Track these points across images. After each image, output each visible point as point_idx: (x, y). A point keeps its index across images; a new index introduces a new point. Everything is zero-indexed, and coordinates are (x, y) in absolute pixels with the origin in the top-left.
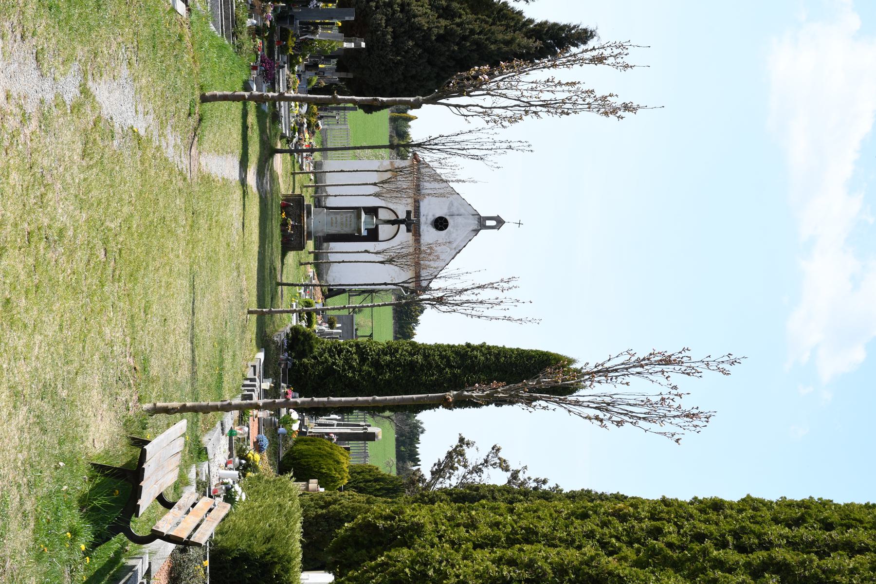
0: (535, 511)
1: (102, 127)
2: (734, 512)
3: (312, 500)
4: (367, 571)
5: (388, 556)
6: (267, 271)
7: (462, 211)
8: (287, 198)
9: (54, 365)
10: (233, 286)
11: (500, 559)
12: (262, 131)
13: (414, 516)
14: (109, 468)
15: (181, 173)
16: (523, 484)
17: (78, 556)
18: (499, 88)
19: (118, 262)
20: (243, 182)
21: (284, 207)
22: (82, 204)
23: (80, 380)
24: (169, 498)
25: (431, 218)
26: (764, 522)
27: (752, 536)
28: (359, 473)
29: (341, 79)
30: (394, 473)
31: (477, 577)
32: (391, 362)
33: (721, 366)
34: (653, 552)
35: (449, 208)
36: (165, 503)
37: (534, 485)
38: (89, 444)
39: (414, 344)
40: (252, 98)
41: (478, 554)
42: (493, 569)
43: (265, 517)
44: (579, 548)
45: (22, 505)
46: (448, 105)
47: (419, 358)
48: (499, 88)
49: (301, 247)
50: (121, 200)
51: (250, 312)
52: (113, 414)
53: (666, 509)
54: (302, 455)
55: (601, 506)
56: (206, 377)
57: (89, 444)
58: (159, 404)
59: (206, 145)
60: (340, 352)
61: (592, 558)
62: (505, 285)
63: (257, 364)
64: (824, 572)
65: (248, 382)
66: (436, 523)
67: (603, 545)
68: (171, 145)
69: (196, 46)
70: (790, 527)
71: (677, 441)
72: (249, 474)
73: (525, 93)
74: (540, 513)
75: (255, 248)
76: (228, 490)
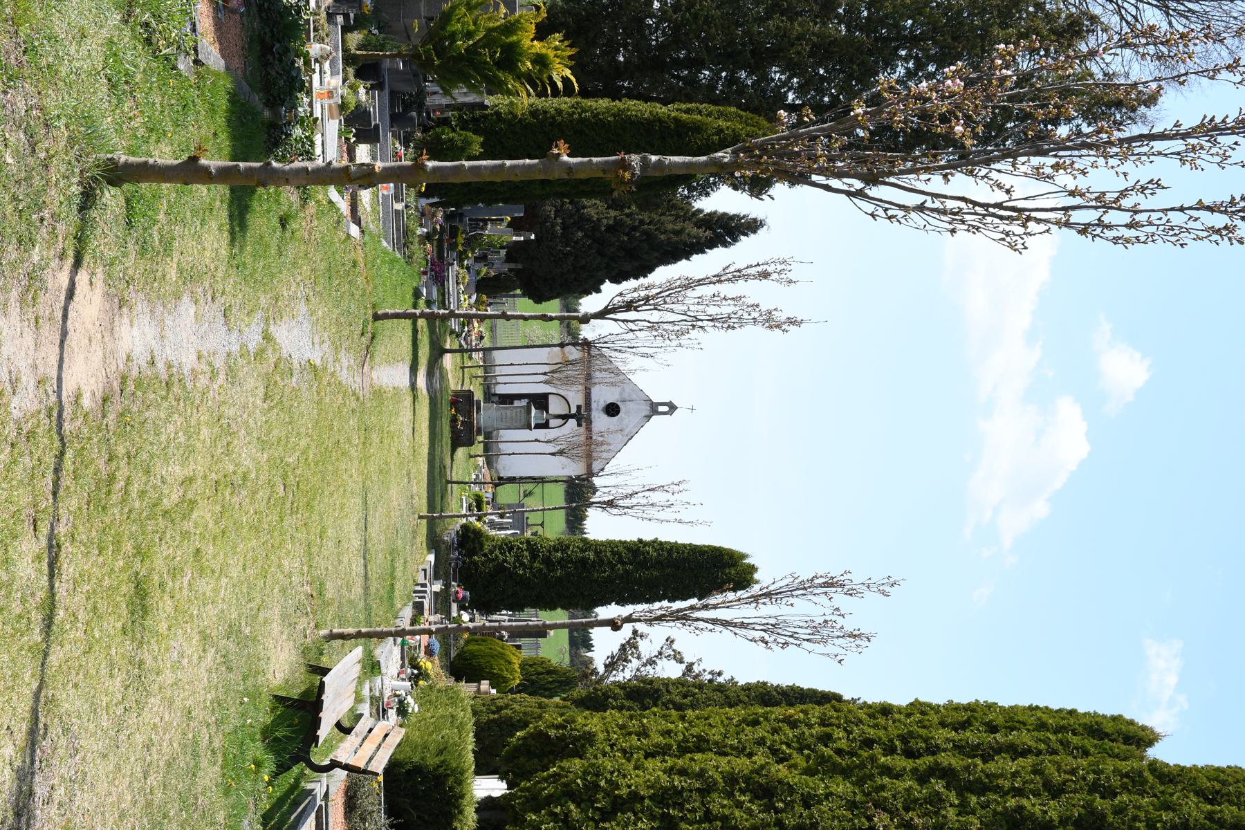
0: (706, 719)
1: (283, 367)
2: (902, 717)
3: (484, 705)
4: (539, 782)
5: (560, 767)
6: (437, 471)
7: (634, 397)
8: (457, 394)
9: (239, 604)
10: (405, 492)
11: (672, 768)
12: (432, 332)
13: (586, 725)
14: (290, 699)
15: (354, 394)
16: (697, 676)
17: (261, 786)
18: (665, 303)
19: (296, 494)
20: (413, 386)
21: (454, 403)
22: (263, 444)
23: (262, 615)
24: (346, 724)
25: (602, 404)
26: (931, 726)
27: (919, 741)
28: (531, 666)
29: (510, 270)
30: (567, 660)
31: (648, 787)
32: (562, 559)
33: (881, 588)
34: (822, 760)
36: (343, 729)
37: (709, 677)
38: (270, 676)
39: (585, 541)
40: (423, 315)
41: (649, 764)
42: (664, 779)
43: (437, 729)
44: (750, 755)
45: (211, 743)
46: (616, 320)
47: (591, 555)
48: (665, 303)
49: (470, 443)
50: (299, 434)
51: (420, 517)
52: (292, 643)
53: (835, 714)
54: (474, 655)
55: (772, 712)
56: (377, 590)
57: (270, 676)
58: (335, 631)
59: (377, 359)
60: (510, 549)
61: (762, 767)
62: (676, 488)
63: (428, 568)
64: (987, 776)
65: (419, 588)
66: (608, 732)
67: (774, 751)
68: (345, 369)
69: (369, 266)
70: (956, 730)
71: (840, 662)
72: (421, 683)
73: (692, 308)
74: (711, 721)
75: (425, 450)
76: (401, 702)
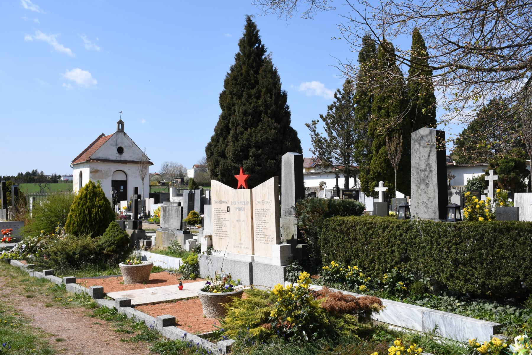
7: (115, 140)
25: (118, 155)
35: (113, 146)
